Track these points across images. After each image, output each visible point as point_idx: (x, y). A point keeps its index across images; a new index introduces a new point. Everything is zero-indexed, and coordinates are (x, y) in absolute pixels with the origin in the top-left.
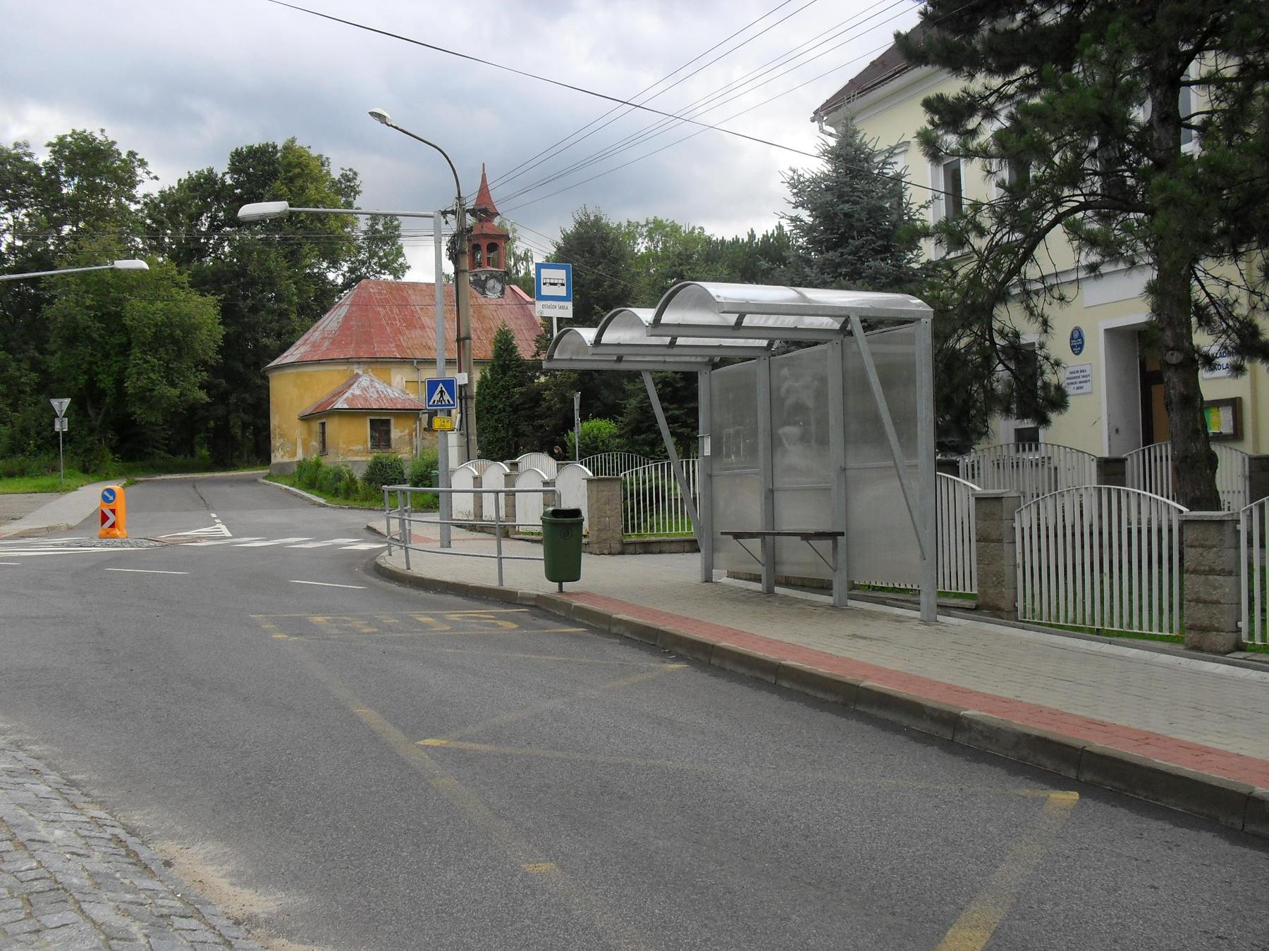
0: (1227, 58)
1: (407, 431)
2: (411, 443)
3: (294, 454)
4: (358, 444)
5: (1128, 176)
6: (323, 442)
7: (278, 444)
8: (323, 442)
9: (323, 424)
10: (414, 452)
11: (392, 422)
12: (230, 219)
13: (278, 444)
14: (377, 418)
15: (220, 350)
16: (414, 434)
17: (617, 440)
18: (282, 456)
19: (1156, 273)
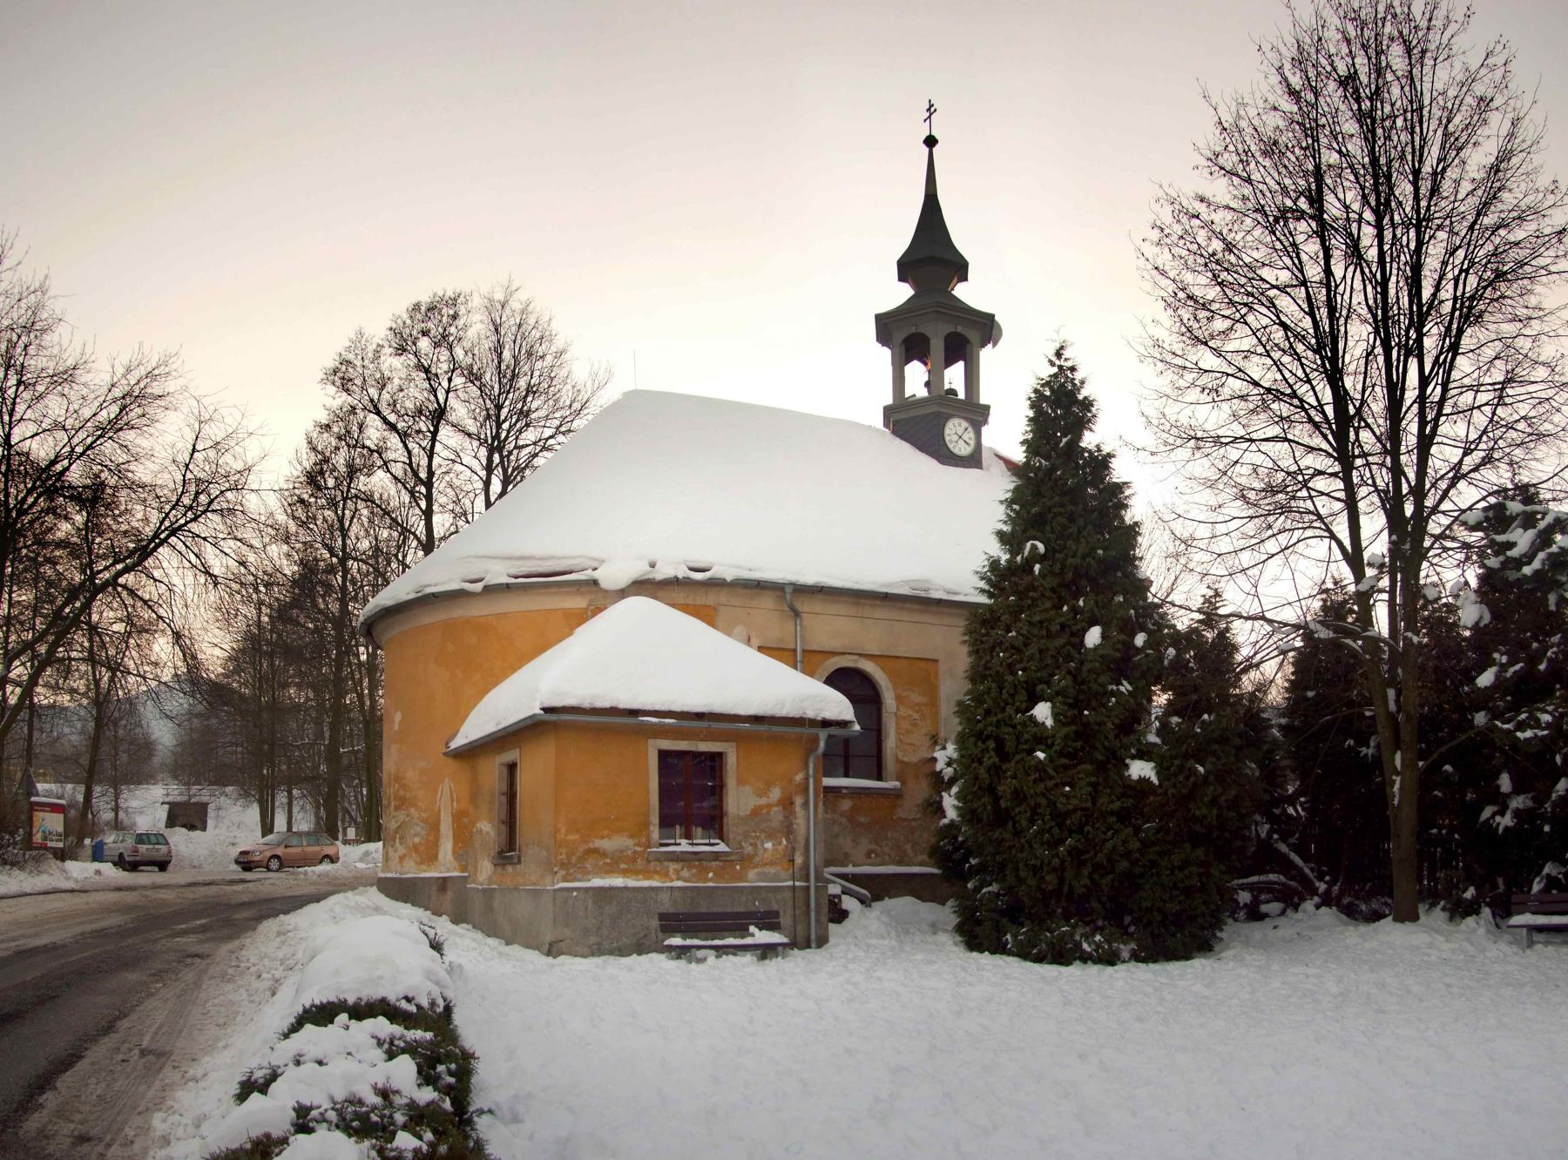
0: (475, 1059)
1: (776, 794)
2: (789, 831)
3: (431, 856)
4: (619, 831)
5: (1493, 816)
6: (510, 822)
7: (393, 825)
8: (510, 822)
9: (512, 767)
10: (799, 860)
11: (731, 760)
12: (1317, 647)
13: (393, 825)
14: (683, 745)
15: (1477, 913)
16: (799, 800)
17: (19, 775)
18: (402, 858)
19: (1513, 824)
